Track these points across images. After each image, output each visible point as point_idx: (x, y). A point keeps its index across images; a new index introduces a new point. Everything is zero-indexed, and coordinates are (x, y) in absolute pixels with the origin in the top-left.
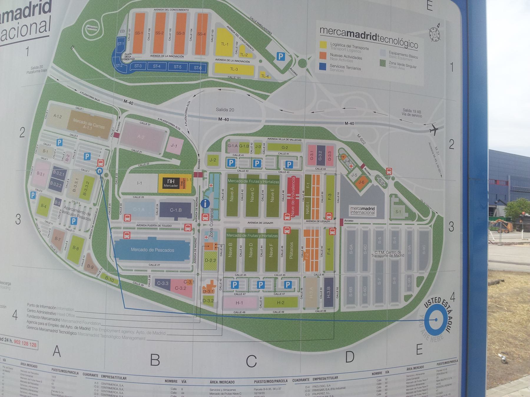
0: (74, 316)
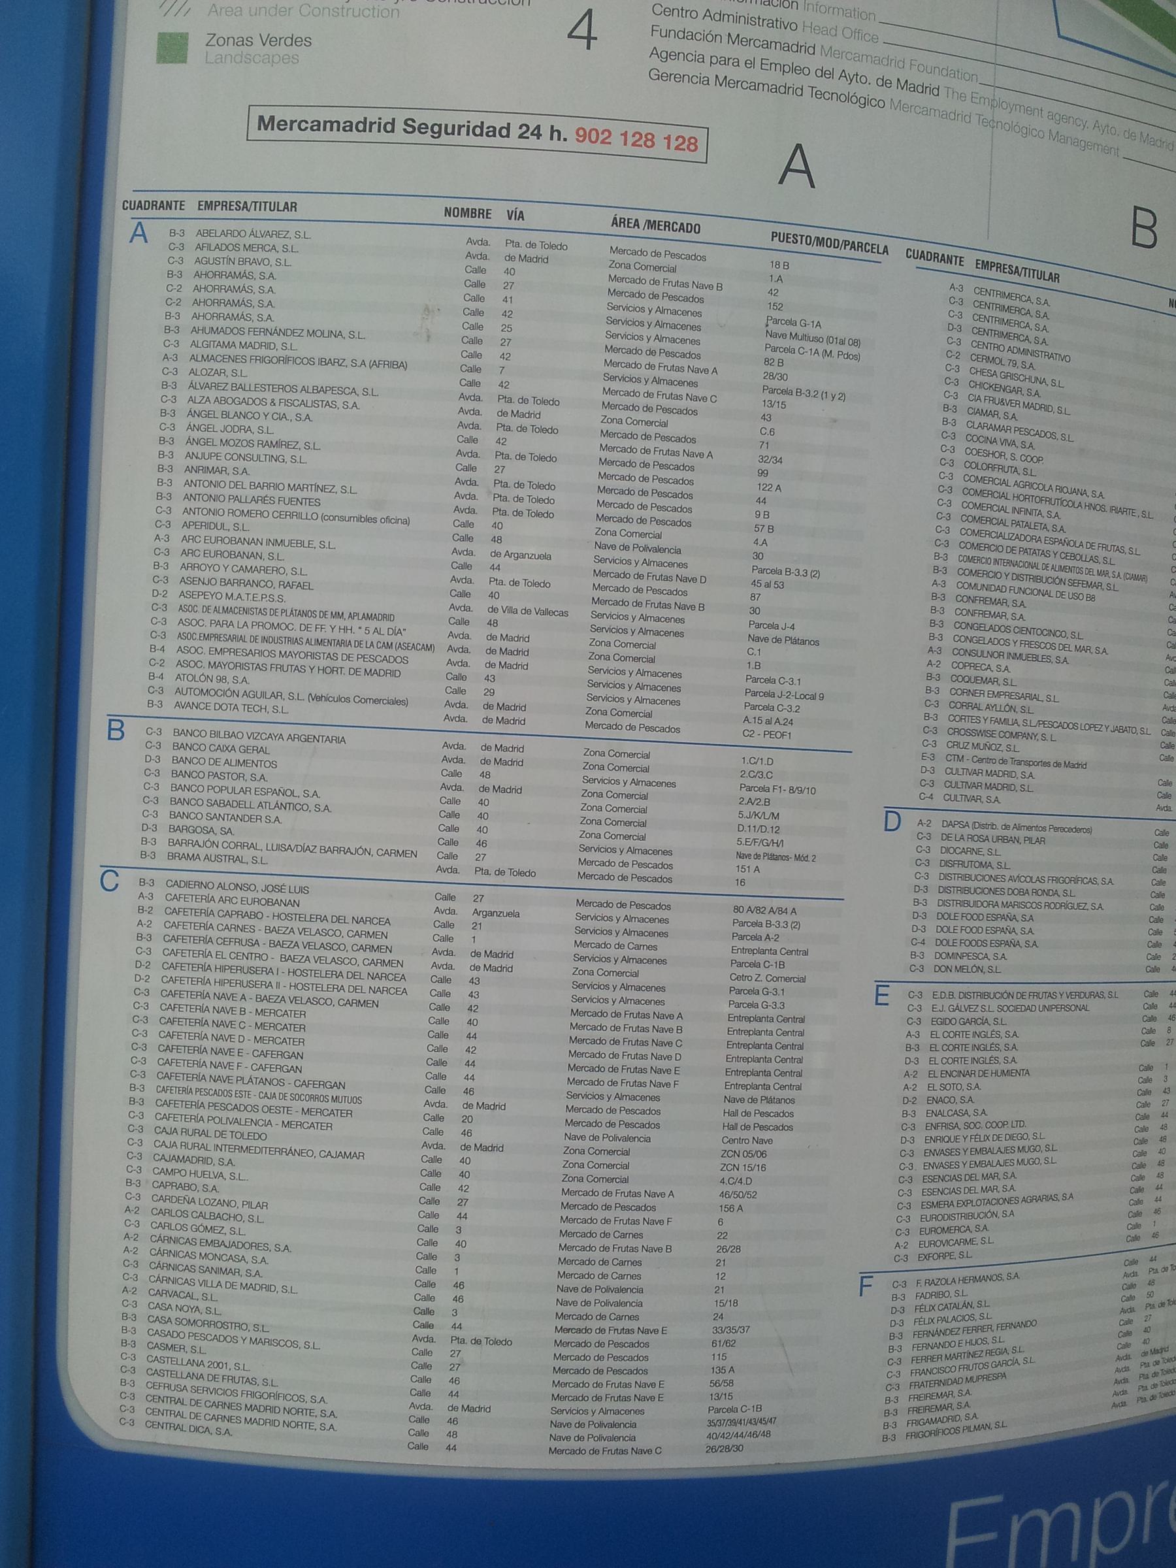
0: (874, 39)
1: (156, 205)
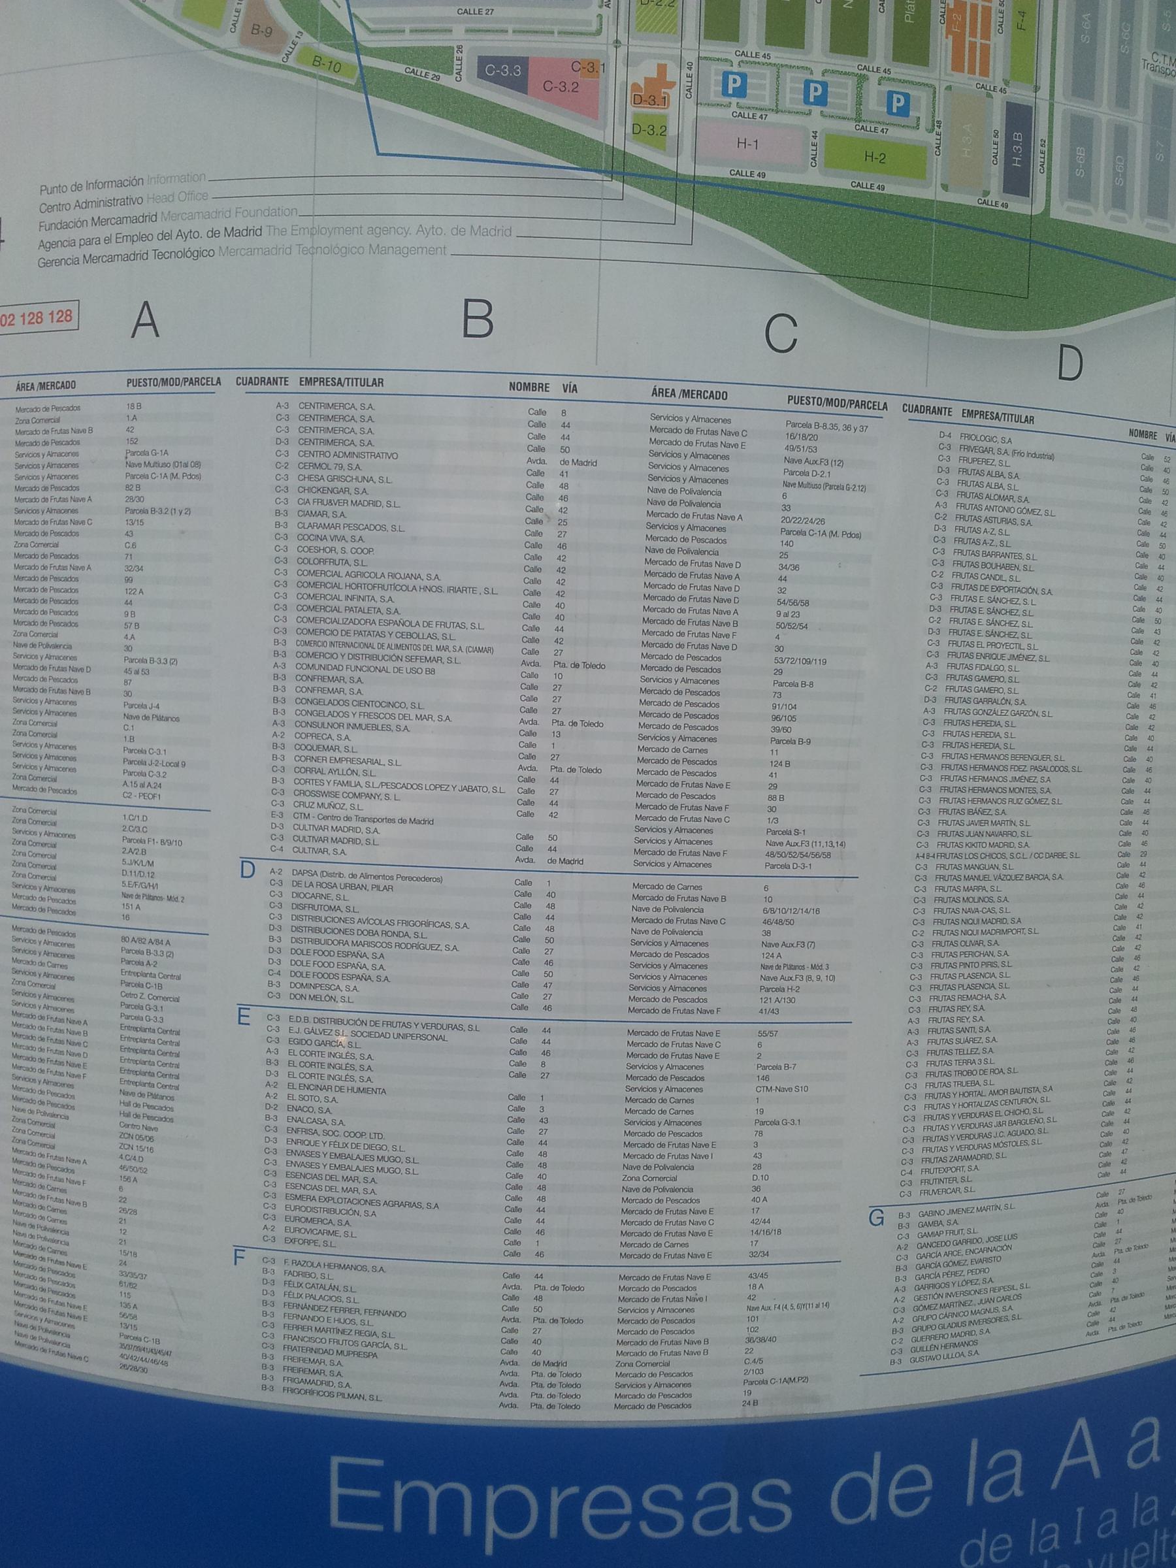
0: (204, 196)
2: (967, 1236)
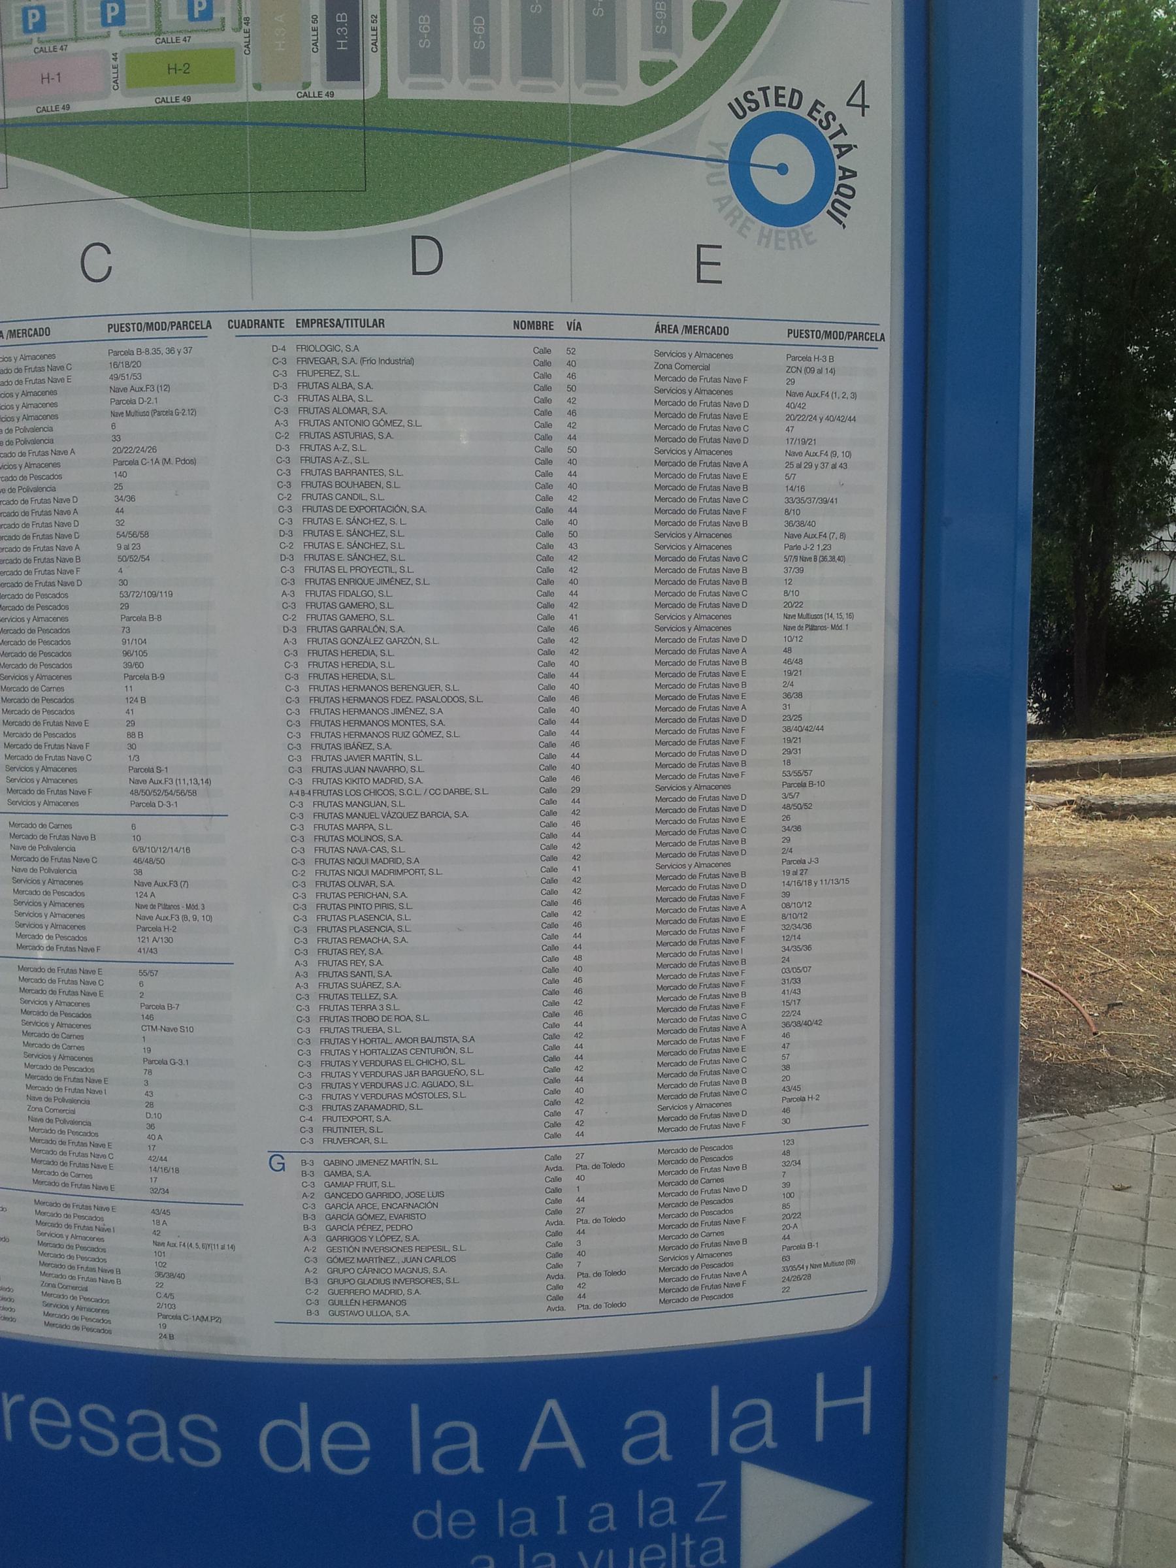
1: (258, 324)
2: (382, 1190)
